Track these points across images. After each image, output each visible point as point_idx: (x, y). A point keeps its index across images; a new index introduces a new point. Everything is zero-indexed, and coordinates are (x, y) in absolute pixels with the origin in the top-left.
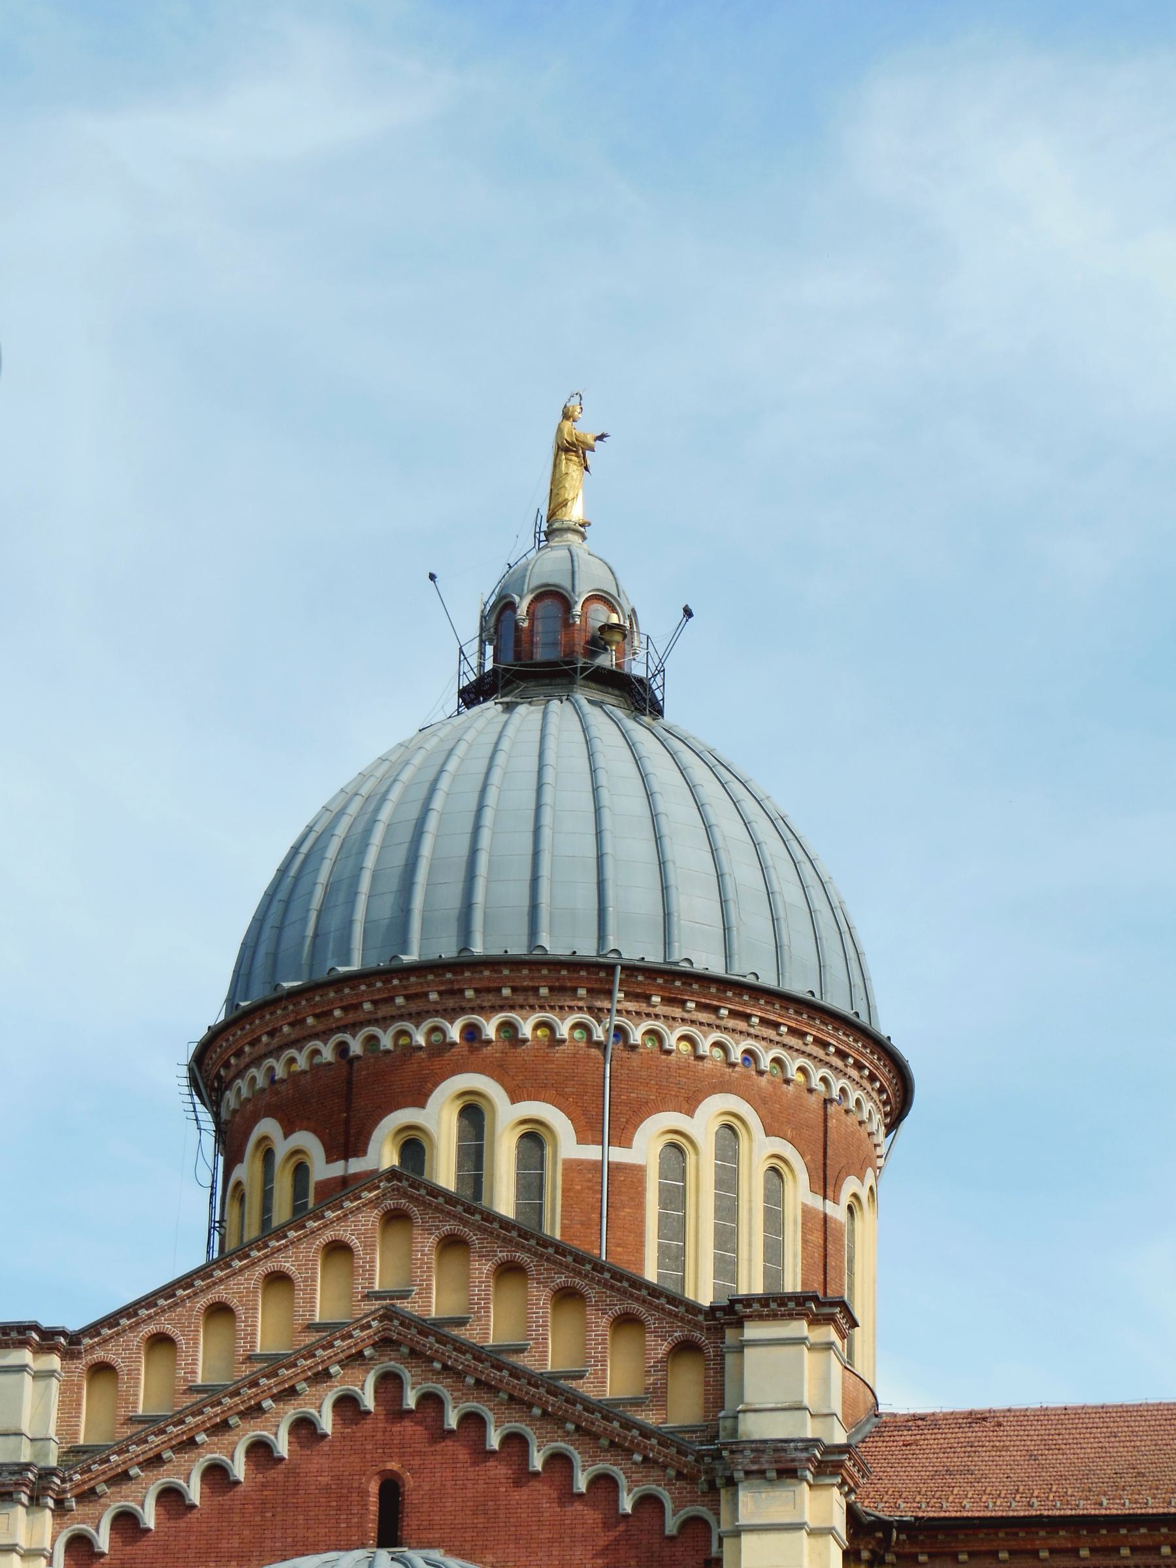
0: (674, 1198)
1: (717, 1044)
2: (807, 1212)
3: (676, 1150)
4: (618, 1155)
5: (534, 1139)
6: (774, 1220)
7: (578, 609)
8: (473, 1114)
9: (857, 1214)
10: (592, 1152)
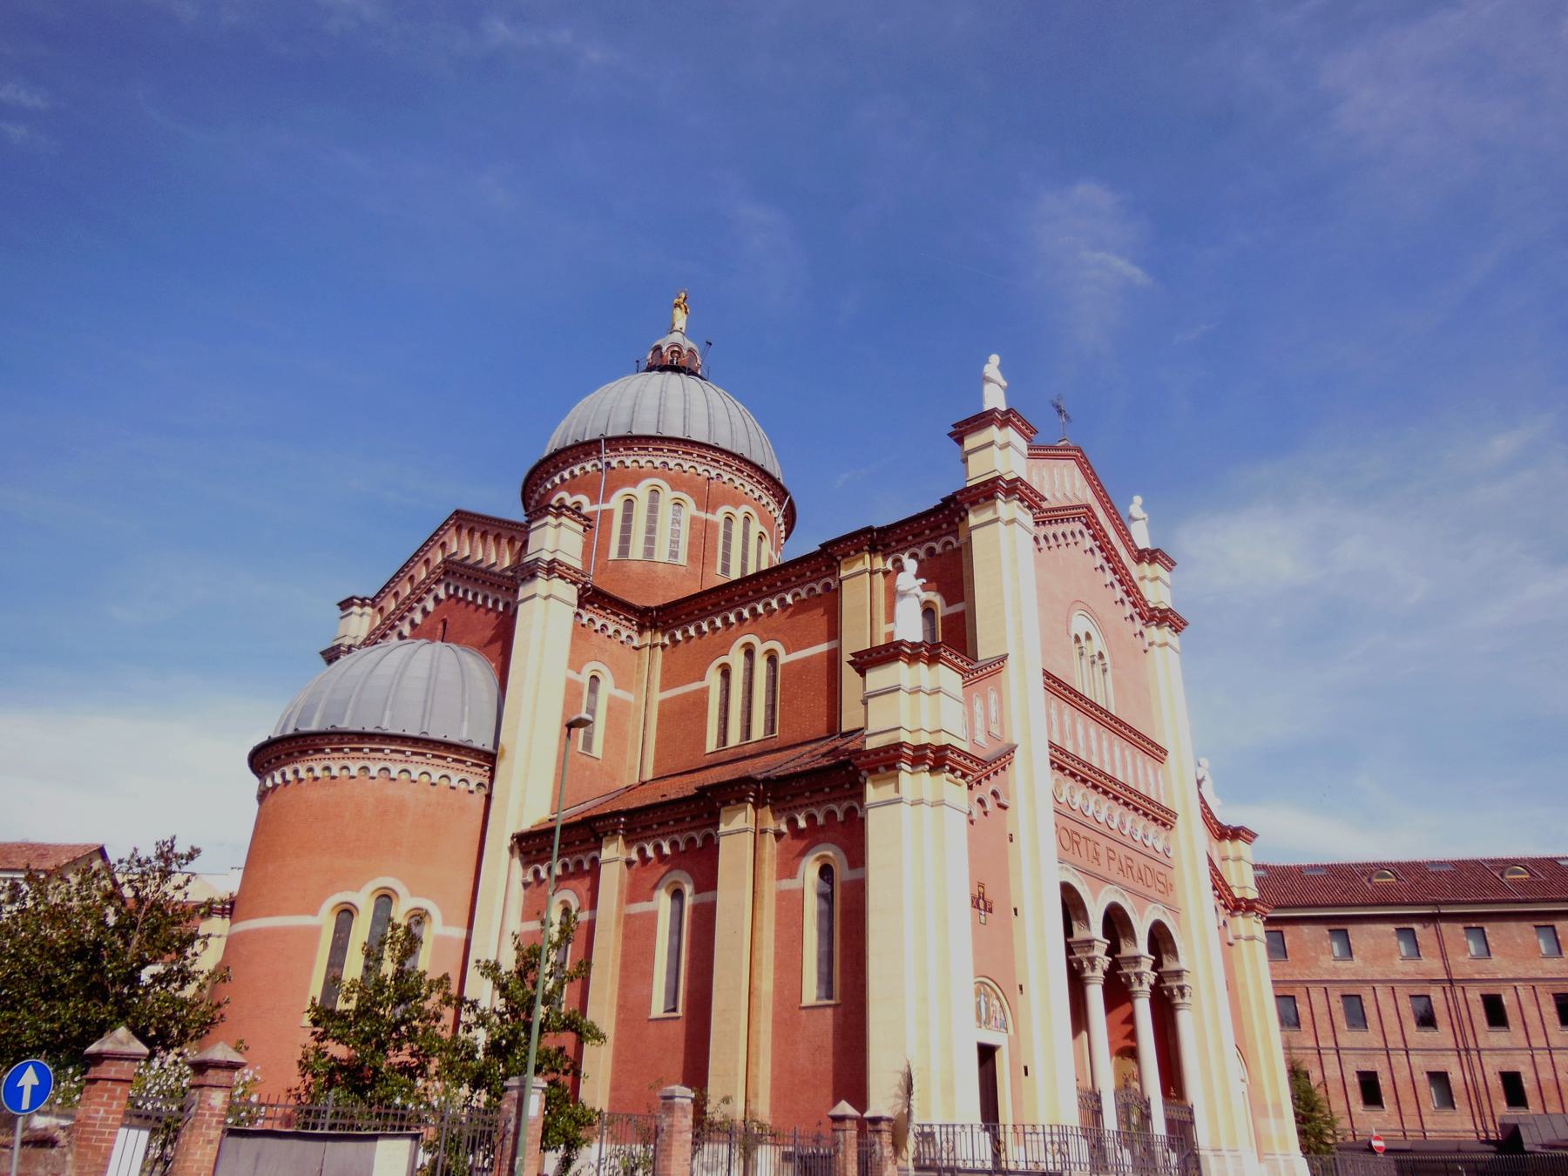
0: (627, 518)
3: (629, 503)
5: (772, 658)
10: (595, 508)
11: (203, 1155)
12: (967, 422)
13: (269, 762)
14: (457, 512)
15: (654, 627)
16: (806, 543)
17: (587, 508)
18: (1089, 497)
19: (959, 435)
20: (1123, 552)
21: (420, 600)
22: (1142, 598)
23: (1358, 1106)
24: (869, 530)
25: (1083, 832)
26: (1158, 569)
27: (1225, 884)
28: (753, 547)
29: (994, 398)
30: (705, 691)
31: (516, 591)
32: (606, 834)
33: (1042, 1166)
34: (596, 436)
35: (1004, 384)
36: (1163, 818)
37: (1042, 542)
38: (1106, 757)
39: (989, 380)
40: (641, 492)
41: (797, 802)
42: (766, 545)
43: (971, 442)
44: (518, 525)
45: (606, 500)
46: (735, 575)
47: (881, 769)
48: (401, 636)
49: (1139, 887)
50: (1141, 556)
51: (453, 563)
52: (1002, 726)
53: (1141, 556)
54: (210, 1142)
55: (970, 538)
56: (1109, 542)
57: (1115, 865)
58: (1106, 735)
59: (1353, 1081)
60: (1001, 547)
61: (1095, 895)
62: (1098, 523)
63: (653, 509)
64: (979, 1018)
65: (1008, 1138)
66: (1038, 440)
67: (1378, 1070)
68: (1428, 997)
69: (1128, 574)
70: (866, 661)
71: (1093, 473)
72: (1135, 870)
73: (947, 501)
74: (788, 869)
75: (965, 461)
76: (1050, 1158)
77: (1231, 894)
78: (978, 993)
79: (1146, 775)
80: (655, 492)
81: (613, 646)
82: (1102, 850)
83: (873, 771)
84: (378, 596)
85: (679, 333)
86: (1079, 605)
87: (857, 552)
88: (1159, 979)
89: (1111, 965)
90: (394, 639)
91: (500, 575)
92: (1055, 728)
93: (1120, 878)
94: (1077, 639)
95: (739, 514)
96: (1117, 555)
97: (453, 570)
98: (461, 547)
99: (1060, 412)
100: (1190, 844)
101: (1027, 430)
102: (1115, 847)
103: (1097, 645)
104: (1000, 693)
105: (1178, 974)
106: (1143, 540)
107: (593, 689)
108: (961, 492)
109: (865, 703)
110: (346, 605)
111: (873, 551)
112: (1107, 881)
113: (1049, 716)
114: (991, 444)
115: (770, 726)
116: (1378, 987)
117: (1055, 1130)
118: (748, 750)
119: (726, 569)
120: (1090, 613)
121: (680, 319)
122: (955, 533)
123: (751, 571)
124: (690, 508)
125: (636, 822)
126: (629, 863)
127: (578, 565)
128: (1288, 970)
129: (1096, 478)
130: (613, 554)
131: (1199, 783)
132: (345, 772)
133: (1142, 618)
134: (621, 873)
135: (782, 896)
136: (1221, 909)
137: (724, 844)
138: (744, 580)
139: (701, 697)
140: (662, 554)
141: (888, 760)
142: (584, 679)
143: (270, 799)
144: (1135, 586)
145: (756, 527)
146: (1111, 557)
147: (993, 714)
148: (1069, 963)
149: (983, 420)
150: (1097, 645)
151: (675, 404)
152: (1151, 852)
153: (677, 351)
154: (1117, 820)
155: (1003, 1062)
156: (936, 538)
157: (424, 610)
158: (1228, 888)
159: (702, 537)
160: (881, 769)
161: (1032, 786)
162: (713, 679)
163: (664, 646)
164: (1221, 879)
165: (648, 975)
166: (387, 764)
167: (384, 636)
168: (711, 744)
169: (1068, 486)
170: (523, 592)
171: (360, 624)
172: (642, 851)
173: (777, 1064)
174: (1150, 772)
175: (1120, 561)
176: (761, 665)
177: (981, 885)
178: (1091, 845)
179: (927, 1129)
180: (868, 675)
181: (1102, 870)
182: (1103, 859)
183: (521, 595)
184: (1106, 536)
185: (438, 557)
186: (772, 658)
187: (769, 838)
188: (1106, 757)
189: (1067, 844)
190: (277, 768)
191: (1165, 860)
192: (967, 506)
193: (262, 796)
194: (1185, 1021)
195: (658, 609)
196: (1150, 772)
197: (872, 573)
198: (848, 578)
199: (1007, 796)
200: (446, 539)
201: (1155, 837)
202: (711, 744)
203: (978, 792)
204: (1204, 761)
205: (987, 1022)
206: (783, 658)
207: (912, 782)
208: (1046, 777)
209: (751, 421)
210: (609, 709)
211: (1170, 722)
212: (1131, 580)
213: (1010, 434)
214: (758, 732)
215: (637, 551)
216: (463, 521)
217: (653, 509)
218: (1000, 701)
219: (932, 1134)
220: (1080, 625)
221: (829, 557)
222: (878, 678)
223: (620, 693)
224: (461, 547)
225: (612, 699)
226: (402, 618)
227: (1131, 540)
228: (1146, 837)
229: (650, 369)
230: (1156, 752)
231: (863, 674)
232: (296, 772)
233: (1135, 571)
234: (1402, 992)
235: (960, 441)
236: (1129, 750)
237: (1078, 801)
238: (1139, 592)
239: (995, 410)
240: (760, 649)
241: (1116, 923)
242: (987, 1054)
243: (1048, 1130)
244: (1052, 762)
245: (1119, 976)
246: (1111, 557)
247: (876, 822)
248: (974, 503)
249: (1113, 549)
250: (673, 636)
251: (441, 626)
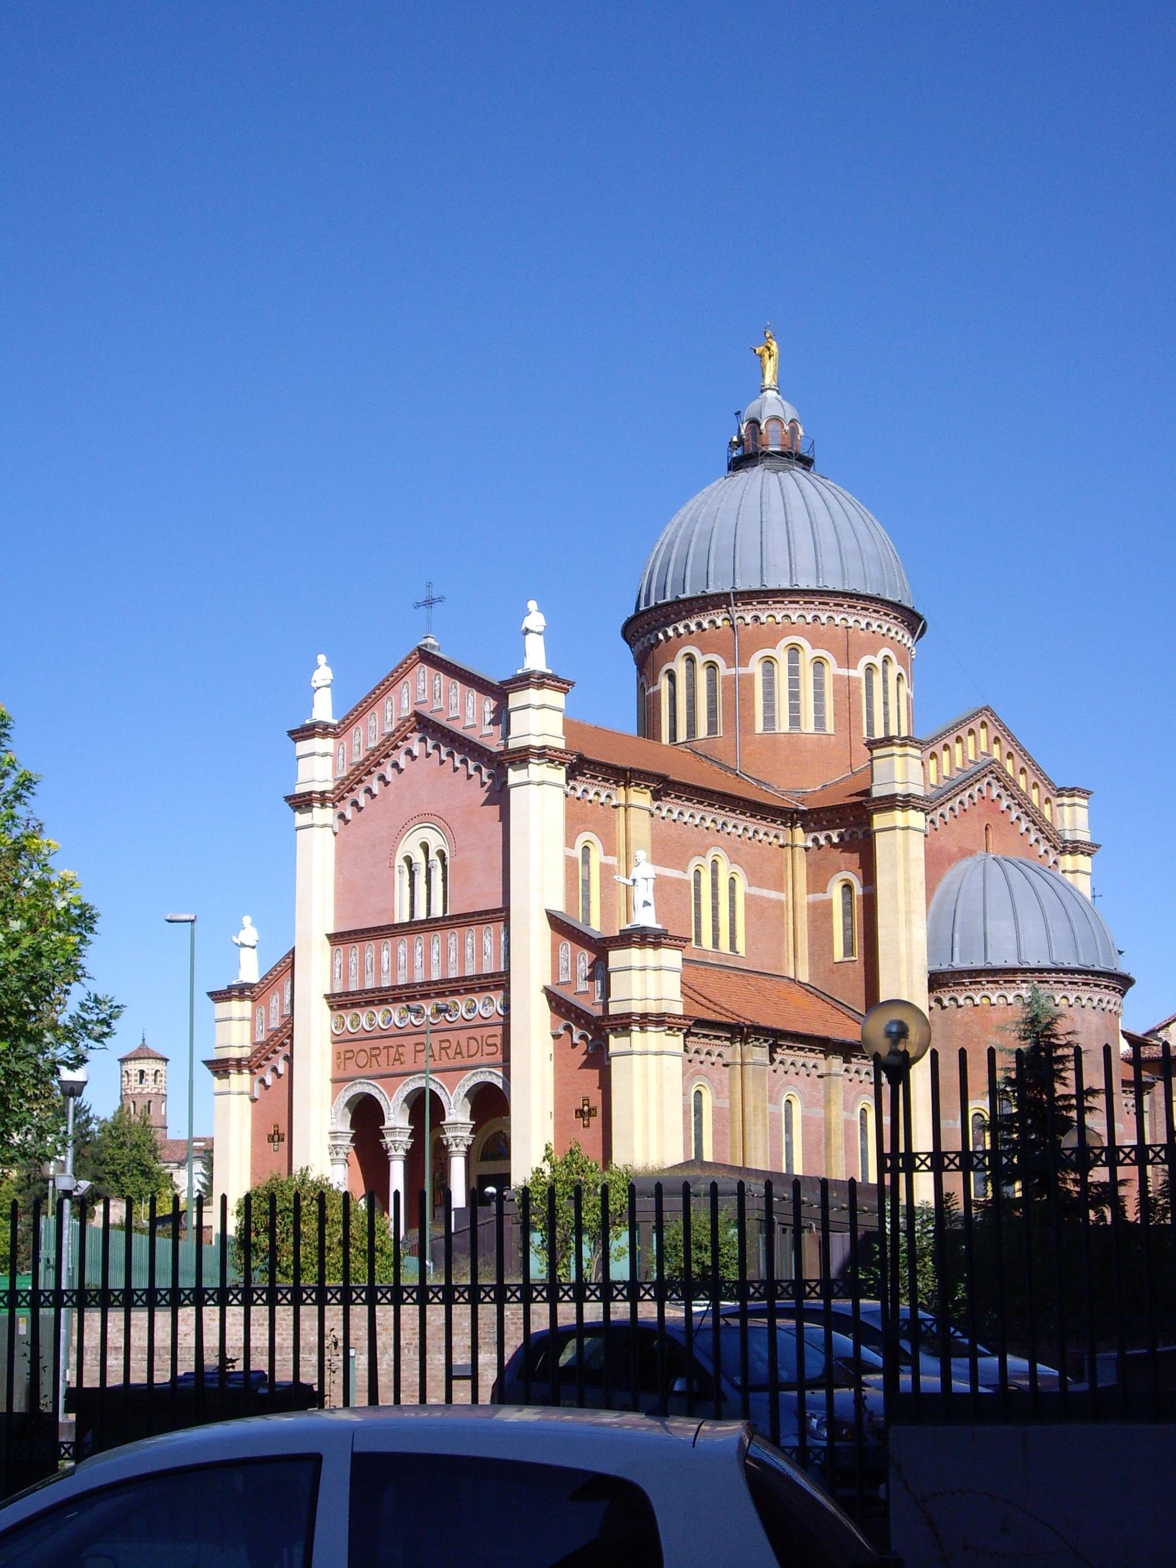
0: (769, 683)
1: (968, 997)
2: (837, 678)
3: (769, 661)
4: (742, 670)
5: (712, 666)
6: (819, 685)
7: (762, 427)
8: (690, 659)
9: (990, 831)
10: (732, 671)
63: (793, 671)
80: (794, 649)
124: (832, 669)
130: (759, 727)
135: (813, 907)
141: (890, 803)
142: (578, 853)
172: (815, 840)
176: (702, 676)
203: (929, 818)
215: (783, 724)
223: (843, 672)
240: (700, 659)
241: (425, 1109)
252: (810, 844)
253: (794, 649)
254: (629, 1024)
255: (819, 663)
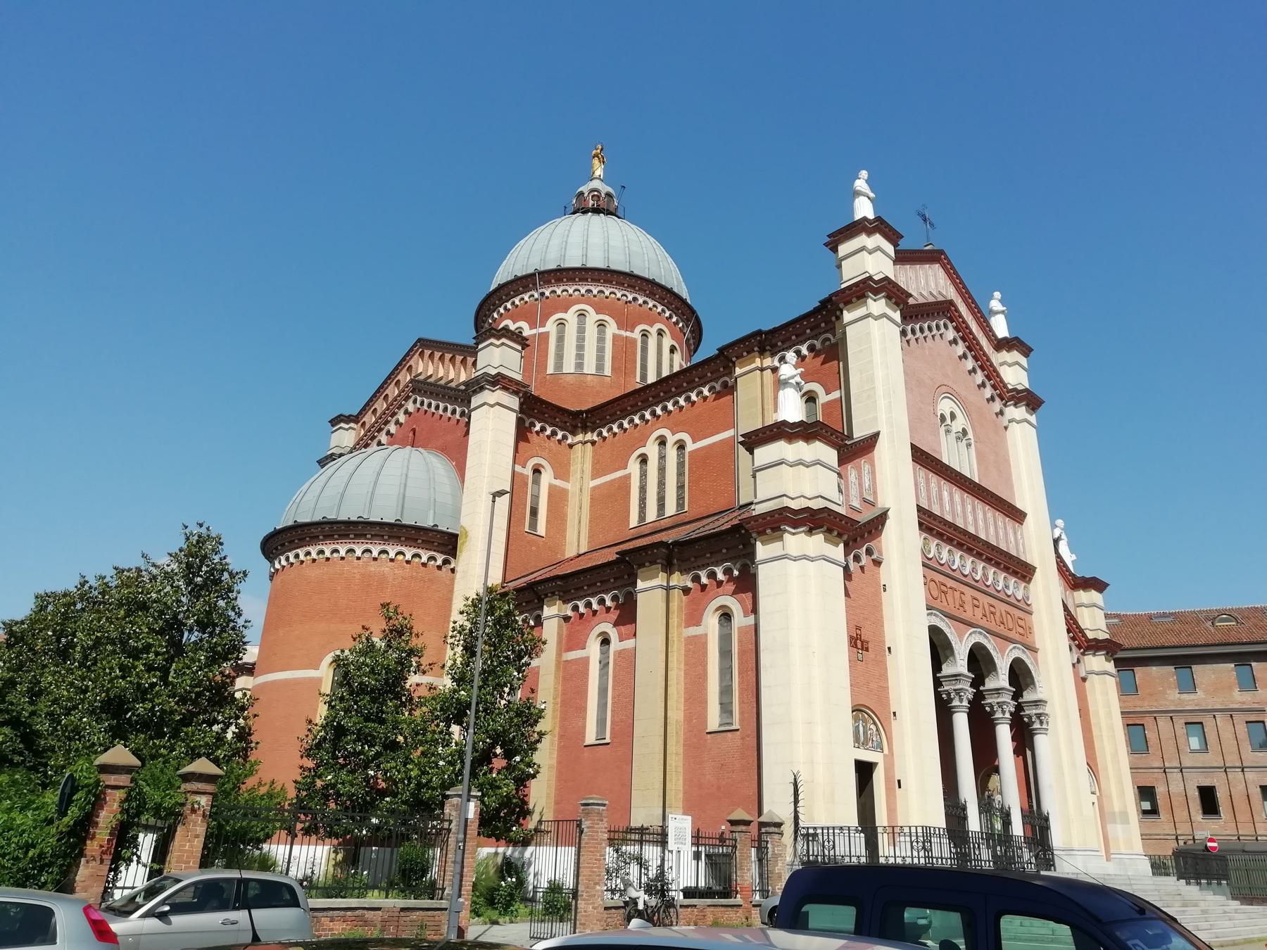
0: (561, 339)
3: (561, 324)
4: (542, 330)
5: (681, 446)
10: (534, 331)
11: (191, 846)
12: (840, 232)
13: (276, 549)
14: (419, 340)
15: (585, 429)
16: (707, 350)
17: (527, 332)
18: (951, 293)
19: (834, 241)
20: (984, 342)
21: (394, 414)
22: (1002, 381)
23: (1198, 816)
24: (759, 333)
25: (950, 583)
26: (1015, 356)
27: (1078, 627)
28: (662, 356)
29: (864, 209)
30: (628, 477)
31: (470, 402)
32: (546, 596)
33: (909, 861)
34: (531, 271)
35: (872, 195)
36: (1024, 571)
37: (910, 336)
38: (970, 518)
39: (858, 194)
40: (571, 316)
41: (700, 562)
42: (677, 357)
43: (844, 249)
44: (468, 347)
45: (543, 325)
46: (652, 378)
47: (768, 531)
48: (379, 444)
49: (1001, 630)
50: (1001, 345)
51: (419, 381)
52: (875, 493)
53: (1001, 345)
54: (197, 836)
55: (844, 333)
56: (971, 333)
57: (979, 612)
58: (969, 499)
59: (1194, 794)
60: (873, 335)
61: (961, 637)
62: (961, 316)
63: (581, 330)
64: (857, 739)
65: (883, 841)
66: (903, 244)
67: (1216, 784)
68: (1263, 722)
69: (988, 360)
70: (752, 441)
71: (955, 272)
72: (998, 614)
73: (824, 303)
74: (694, 618)
75: (839, 267)
76: (915, 854)
77: (1084, 635)
78: (856, 719)
79: (1006, 534)
80: (582, 315)
81: (552, 444)
82: (967, 598)
83: (762, 533)
84: (360, 413)
85: (598, 182)
86: (944, 389)
87: (748, 353)
88: (1019, 708)
89: (975, 695)
90: (374, 447)
91: (456, 389)
92: (924, 494)
93: (983, 623)
94: (943, 418)
95: (653, 330)
96: (978, 343)
97: (422, 387)
98: (424, 367)
99: (925, 220)
100: (1046, 593)
101: (893, 236)
102: (977, 595)
103: (960, 423)
104: (873, 465)
105: (1037, 703)
106: (1001, 328)
107: (536, 482)
108: (836, 294)
109: (754, 477)
110: (335, 421)
111: (762, 352)
112: (971, 625)
113: (916, 484)
114: (863, 249)
115: (680, 504)
116: (1218, 715)
117: (920, 830)
118: (664, 524)
119: (644, 377)
120: (952, 395)
121: (599, 172)
122: (832, 330)
123: (665, 373)
124: (612, 328)
125: (570, 584)
126: (567, 619)
127: (518, 377)
128: (1139, 703)
129: (958, 277)
131: (1056, 542)
132: (335, 555)
133: (1002, 399)
134: (560, 627)
136: (1074, 648)
137: (641, 599)
138: (662, 382)
139: (625, 482)
140: (590, 367)
143: (277, 579)
144: (995, 370)
145: (668, 342)
146: (973, 346)
147: (867, 483)
148: (938, 695)
149: (856, 228)
150: (960, 423)
151: (596, 240)
152: (1012, 600)
153: (595, 193)
154: (980, 572)
155: (879, 778)
156: (818, 332)
157: (397, 422)
158: (1082, 631)
159: (624, 351)
160: (768, 531)
161: (901, 544)
162: (634, 467)
163: (593, 443)
164: (1076, 622)
165: (583, 709)
166: (369, 546)
167: (366, 446)
168: (634, 522)
169: (933, 285)
170: (475, 401)
171: (346, 437)
172: (576, 608)
173: (688, 782)
174: (1010, 532)
175: (981, 349)
176: (671, 453)
177: (858, 628)
178: (957, 594)
179: (811, 831)
180: (756, 451)
181: (967, 616)
182: (968, 607)
183: (474, 404)
184: (968, 327)
185: (405, 377)
186: (681, 446)
187: (676, 593)
188: (970, 518)
189: (935, 593)
190: (282, 554)
191: (1025, 607)
192: (841, 305)
193: (272, 577)
194: (1042, 743)
195: (587, 412)
196: (1010, 532)
197: (762, 370)
198: (741, 375)
199: (880, 552)
200: (411, 363)
201: (1014, 588)
202: (634, 522)
204: (1060, 522)
205: (865, 744)
206: (690, 447)
207: (796, 541)
208: (915, 537)
209: (657, 245)
210: (550, 495)
211: (1027, 485)
212: (992, 365)
213: (878, 240)
214: (671, 509)
215: (569, 366)
216: (424, 344)
217: (581, 330)
218: (873, 473)
219: (815, 835)
220: (946, 406)
221: (726, 359)
222: (765, 454)
223: (558, 483)
224: (424, 367)
225: (551, 487)
226: (380, 430)
227: (991, 330)
228: (1007, 587)
229: (574, 213)
230: (1017, 515)
231: (751, 451)
232: (297, 556)
233: (997, 358)
234: (1240, 719)
235: (835, 250)
236: (990, 513)
237: (945, 556)
238: (998, 375)
239: (865, 219)
240: (671, 439)
241: (980, 662)
242: (864, 771)
243: (913, 830)
244: (920, 524)
245: (983, 706)
246: (973, 346)
247: (766, 575)
248: (848, 303)
249: (975, 338)
250: (600, 434)
251: (411, 434)
252: (570, 613)
253: (582, 315)
254: (463, 396)
255: (601, 325)
